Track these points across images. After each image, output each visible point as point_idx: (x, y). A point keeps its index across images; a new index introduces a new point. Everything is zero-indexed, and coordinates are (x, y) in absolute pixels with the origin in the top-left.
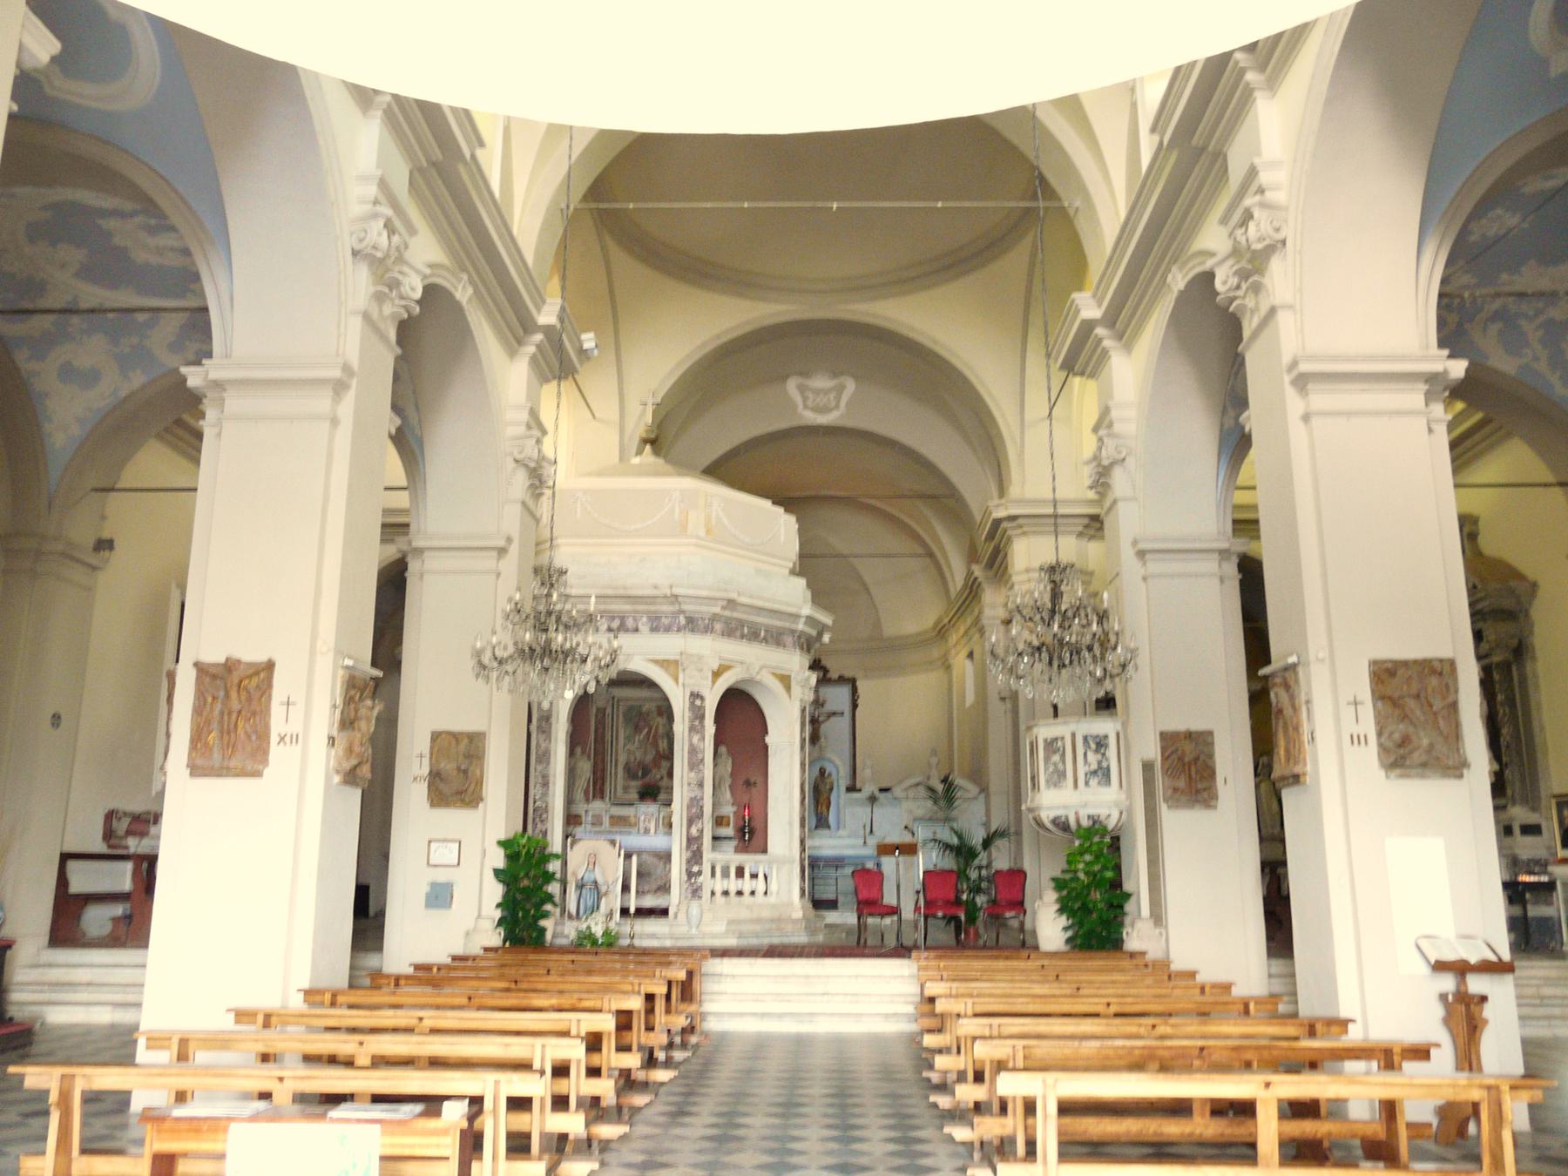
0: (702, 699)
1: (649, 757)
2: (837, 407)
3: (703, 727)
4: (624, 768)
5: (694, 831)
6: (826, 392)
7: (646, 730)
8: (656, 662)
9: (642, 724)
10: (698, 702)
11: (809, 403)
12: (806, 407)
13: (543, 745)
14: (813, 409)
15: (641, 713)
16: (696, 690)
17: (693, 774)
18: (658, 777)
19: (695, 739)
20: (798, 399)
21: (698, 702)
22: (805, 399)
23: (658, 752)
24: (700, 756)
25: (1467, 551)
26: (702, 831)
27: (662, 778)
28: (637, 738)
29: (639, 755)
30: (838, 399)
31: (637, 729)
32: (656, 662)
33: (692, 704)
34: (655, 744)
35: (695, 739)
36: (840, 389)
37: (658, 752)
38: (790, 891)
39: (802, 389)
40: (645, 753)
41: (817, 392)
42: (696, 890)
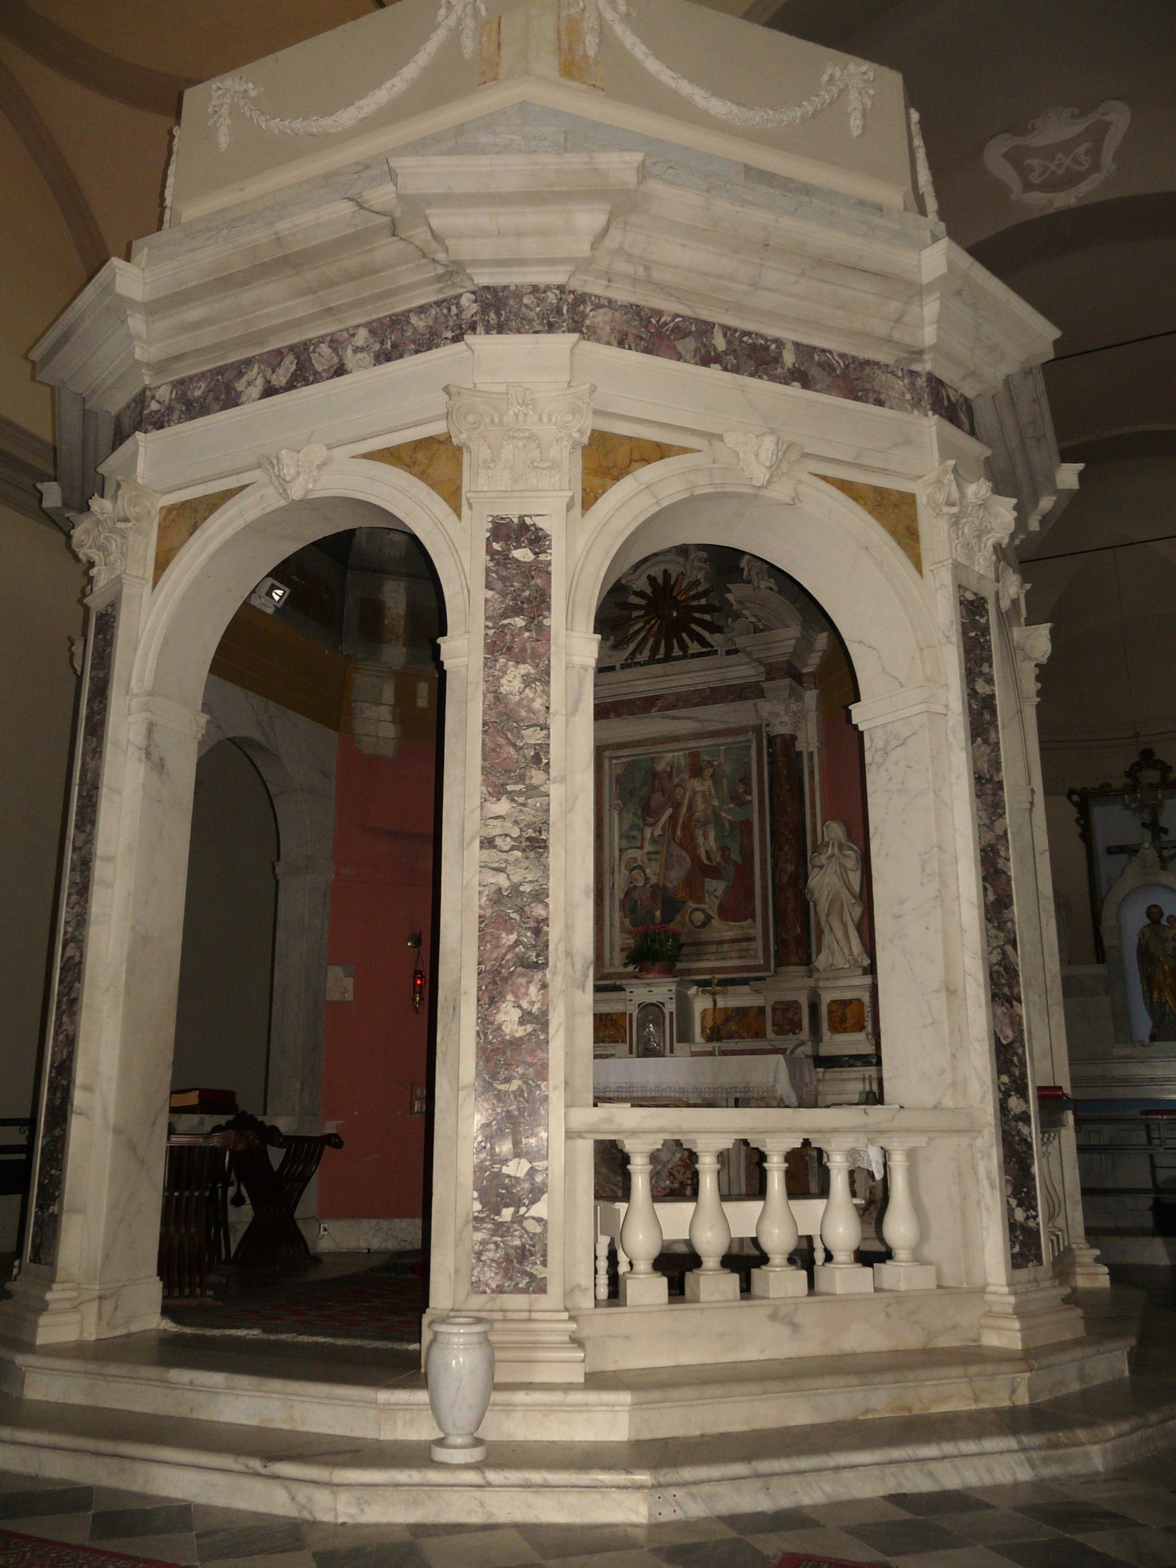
0: (537, 540)
1: (676, 876)
2: (1096, 167)
3: (543, 633)
4: (622, 904)
5: (508, 1017)
6: (1067, 146)
7: (669, 811)
8: (391, 456)
9: (657, 798)
10: (523, 554)
11: (1035, 179)
12: (1028, 187)
13: (91, 765)
14: (1043, 187)
15: (655, 775)
16: (512, 511)
17: (503, 806)
18: (699, 917)
19: (512, 681)
20: (1008, 175)
21: (523, 554)
22: (1024, 172)
23: (696, 859)
24: (532, 736)
25: (755, 1364)
26: (539, 1020)
27: (709, 918)
28: (648, 832)
29: (653, 871)
30: (1095, 153)
31: (648, 812)
32: (391, 456)
33: (500, 560)
34: (689, 844)
35: (512, 681)
36: (1099, 132)
37: (696, 859)
38: (968, 1242)
39: (1014, 158)
40: (667, 866)
41: (1048, 152)
42: (523, 1254)
